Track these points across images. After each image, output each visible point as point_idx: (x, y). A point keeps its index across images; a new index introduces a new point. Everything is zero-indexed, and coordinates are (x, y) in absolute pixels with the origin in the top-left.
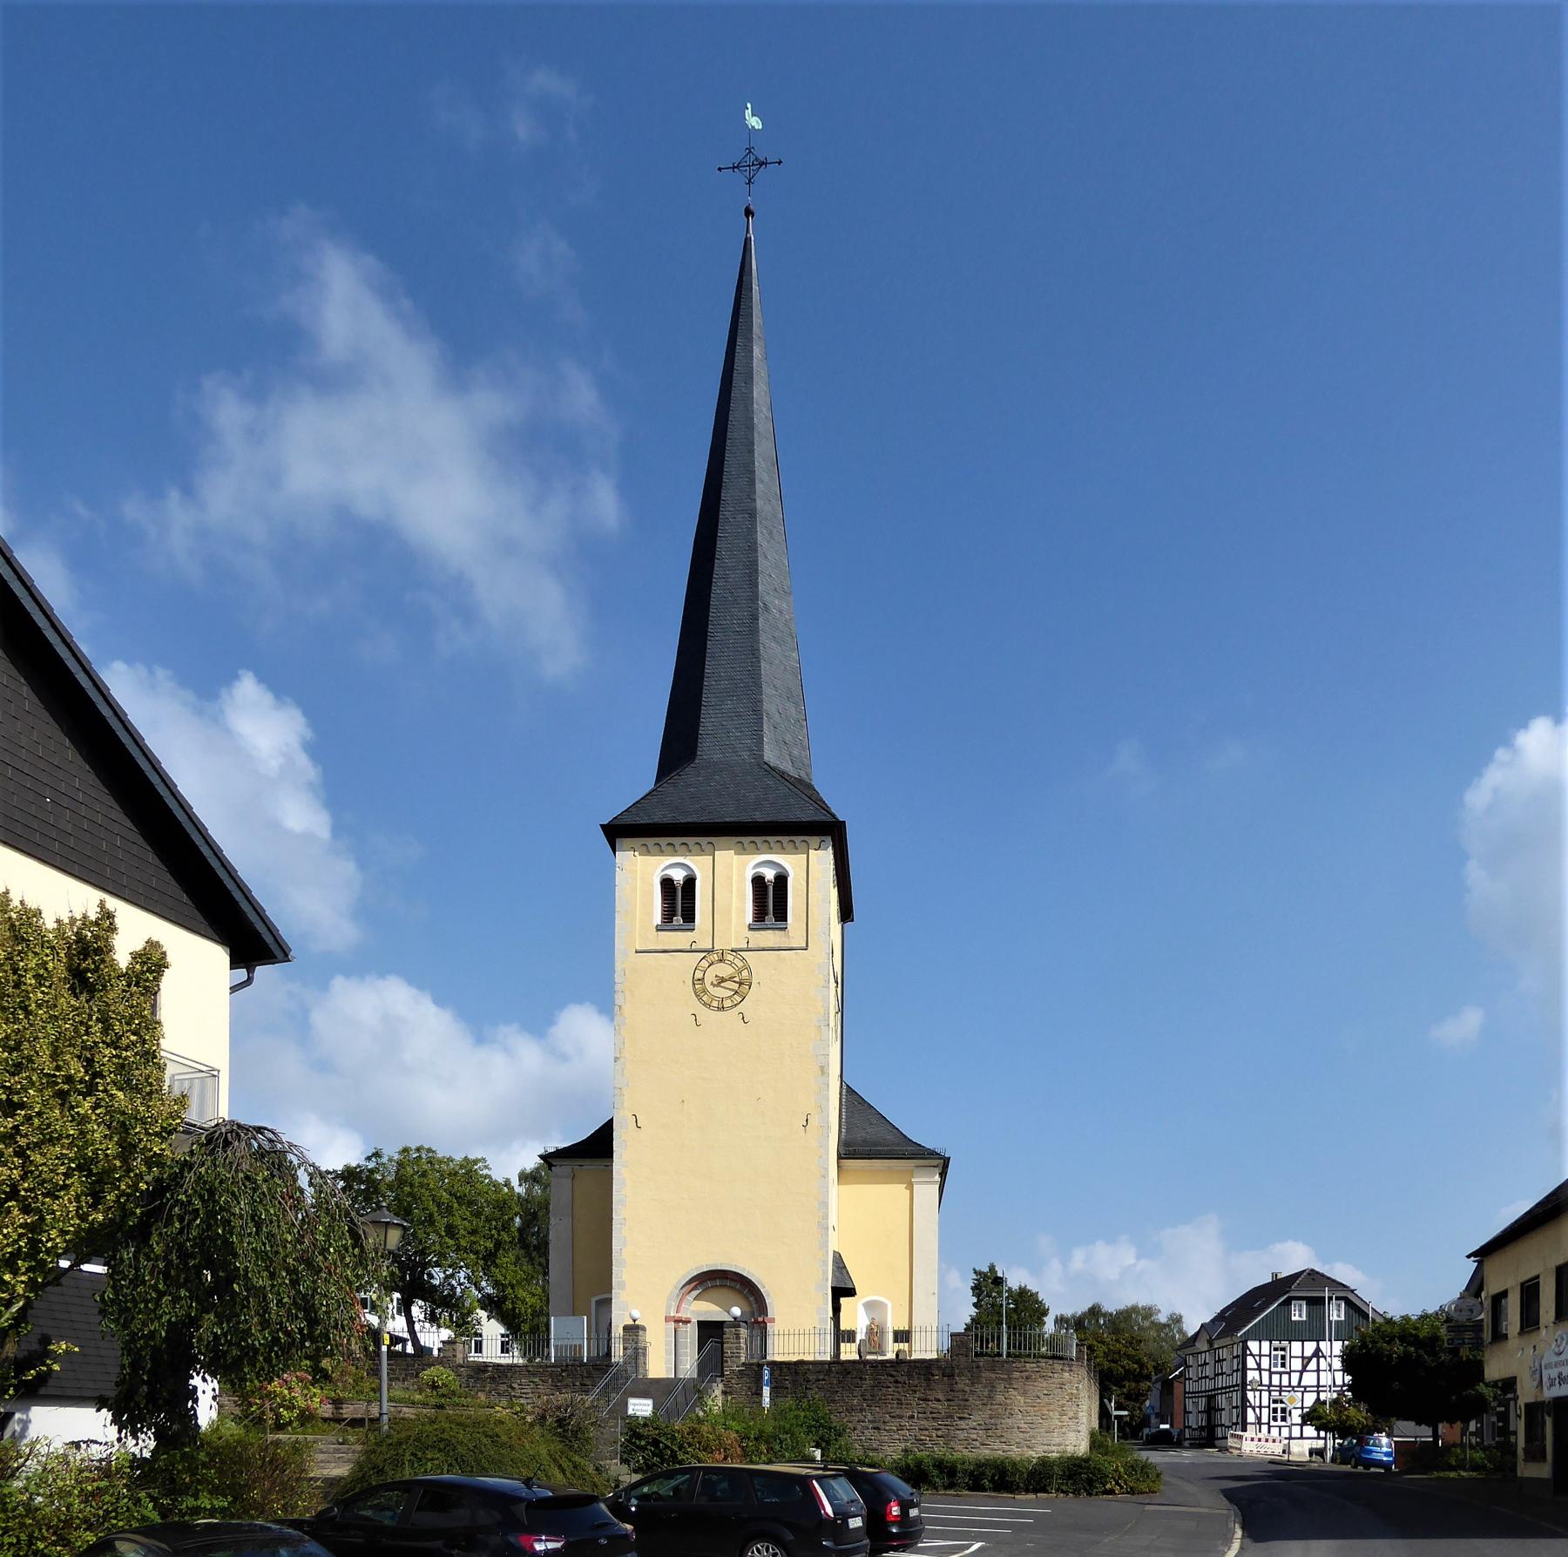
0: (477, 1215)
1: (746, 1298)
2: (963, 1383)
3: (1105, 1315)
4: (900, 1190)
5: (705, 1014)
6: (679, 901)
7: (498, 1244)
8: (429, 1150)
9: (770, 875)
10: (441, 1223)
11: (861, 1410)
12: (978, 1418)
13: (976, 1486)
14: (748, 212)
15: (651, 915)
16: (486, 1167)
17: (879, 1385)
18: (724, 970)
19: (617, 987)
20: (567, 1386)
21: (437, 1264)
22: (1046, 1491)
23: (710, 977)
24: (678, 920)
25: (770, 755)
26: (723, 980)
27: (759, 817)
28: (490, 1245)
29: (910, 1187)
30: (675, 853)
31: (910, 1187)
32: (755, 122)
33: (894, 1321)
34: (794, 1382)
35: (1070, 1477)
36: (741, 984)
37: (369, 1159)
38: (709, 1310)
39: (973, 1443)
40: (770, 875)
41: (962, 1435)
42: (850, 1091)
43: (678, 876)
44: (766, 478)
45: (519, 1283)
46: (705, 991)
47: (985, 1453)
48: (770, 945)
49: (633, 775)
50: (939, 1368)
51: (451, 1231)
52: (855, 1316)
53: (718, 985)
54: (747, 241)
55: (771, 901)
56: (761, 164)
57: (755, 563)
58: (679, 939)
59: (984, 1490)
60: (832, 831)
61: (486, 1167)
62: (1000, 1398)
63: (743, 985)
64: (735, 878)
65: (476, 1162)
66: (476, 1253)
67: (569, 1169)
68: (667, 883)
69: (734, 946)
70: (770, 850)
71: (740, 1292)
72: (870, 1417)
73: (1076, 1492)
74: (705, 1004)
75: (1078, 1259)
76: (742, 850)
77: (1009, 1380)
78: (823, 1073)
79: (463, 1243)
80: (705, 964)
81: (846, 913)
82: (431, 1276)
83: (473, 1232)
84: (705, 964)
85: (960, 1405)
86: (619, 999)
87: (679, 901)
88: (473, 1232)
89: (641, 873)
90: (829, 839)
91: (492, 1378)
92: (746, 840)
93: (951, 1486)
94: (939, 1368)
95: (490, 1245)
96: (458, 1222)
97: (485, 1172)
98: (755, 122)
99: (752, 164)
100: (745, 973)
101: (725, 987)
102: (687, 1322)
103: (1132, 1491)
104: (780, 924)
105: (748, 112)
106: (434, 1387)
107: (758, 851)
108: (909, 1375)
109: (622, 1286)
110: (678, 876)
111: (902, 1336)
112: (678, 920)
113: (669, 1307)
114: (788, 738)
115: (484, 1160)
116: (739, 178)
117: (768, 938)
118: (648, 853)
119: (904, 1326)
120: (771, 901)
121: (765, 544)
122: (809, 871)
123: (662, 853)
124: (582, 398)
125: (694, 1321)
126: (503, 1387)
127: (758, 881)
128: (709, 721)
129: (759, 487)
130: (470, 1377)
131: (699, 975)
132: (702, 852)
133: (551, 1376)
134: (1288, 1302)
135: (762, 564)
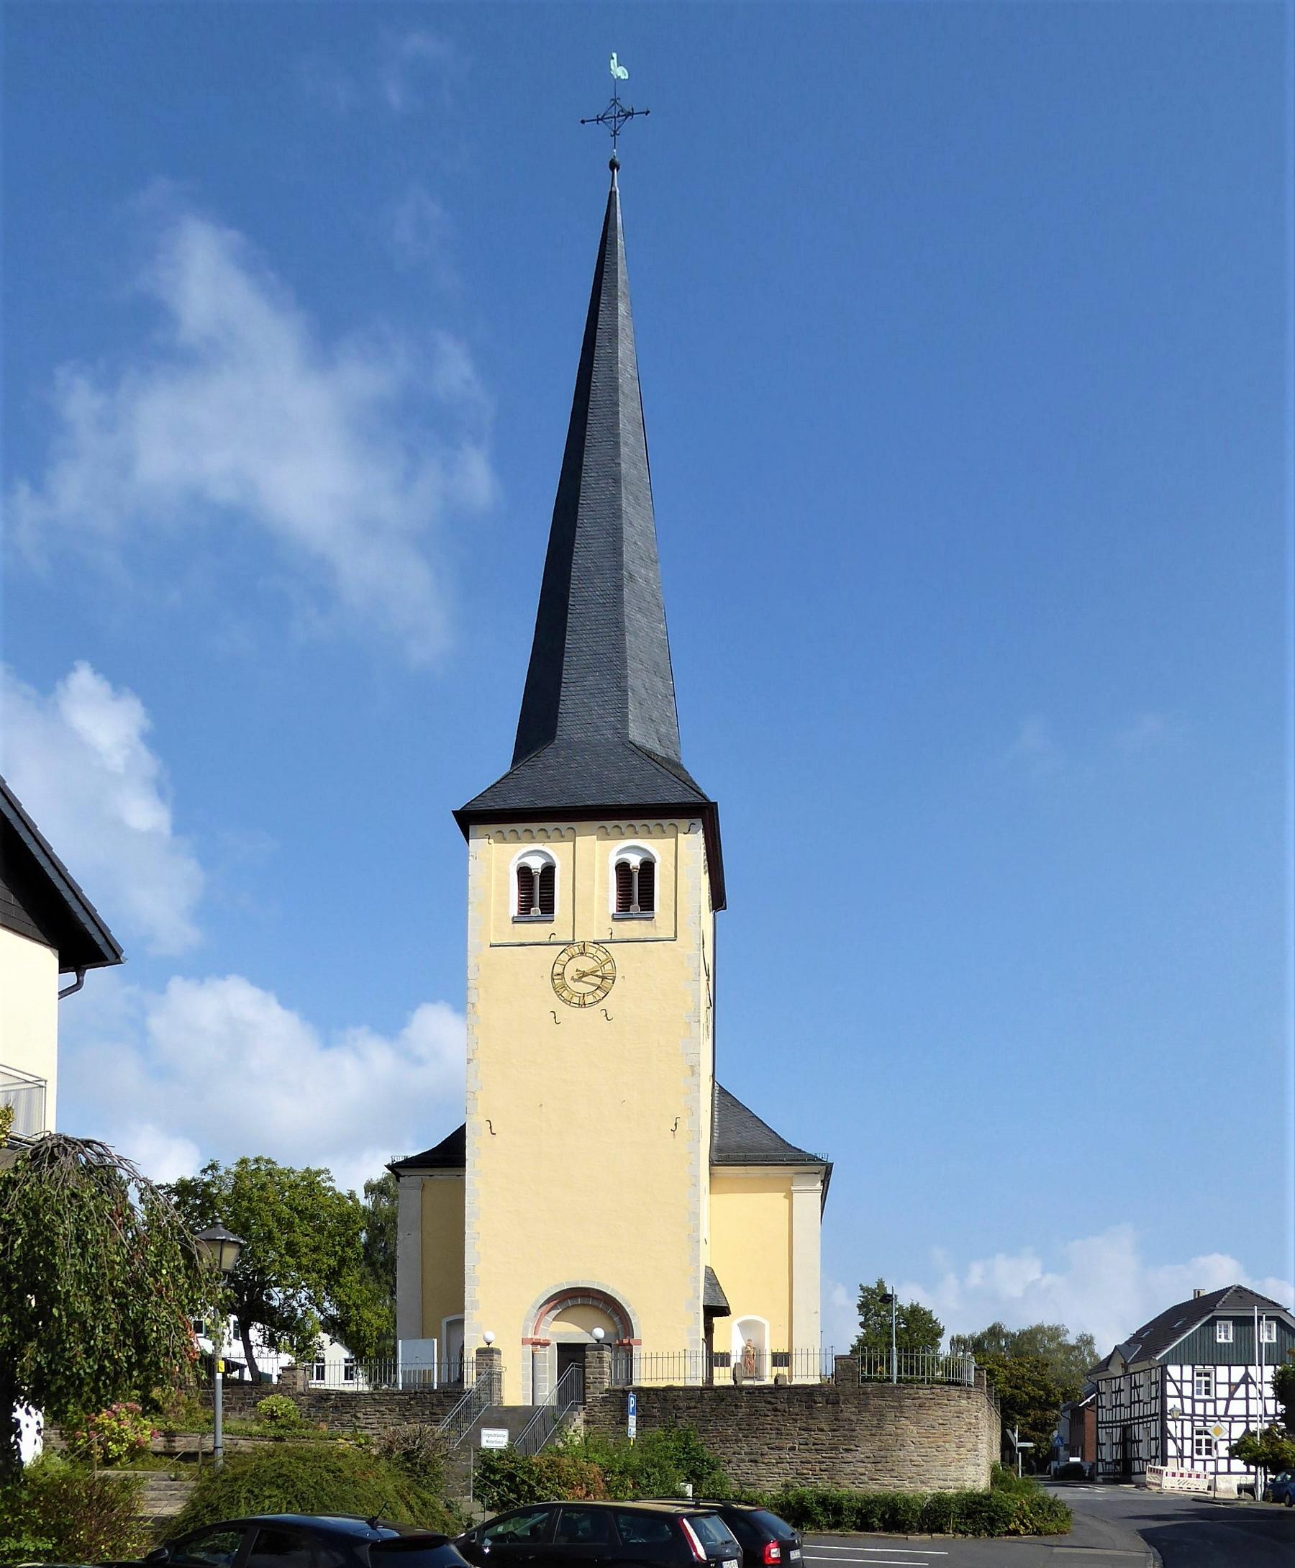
0: (320, 1230)
1: (611, 1318)
2: (848, 1411)
3: (1006, 1336)
4: (776, 1201)
5: (564, 1011)
6: (537, 891)
7: (343, 1261)
9: (635, 861)
10: (281, 1239)
11: (737, 1441)
12: (867, 1449)
13: (865, 1526)
14: (613, 165)
15: (507, 905)
16: (330, 1179)
17: (755, 1413)
18: (586, 964)
19: (470, 984)
22: (942, 1531)
23: (570, 972)
24: (536, 911)
25: (635, 733)
26: (584, 974)
27: (624, 800)
29: (789, 1195)
30: (533, 839)
31: (789, 1195)
32: (620, 72)
33: (772, 1343)
35: (969, 1516)
36: (603, 978)
37: (204, 1171)
39: (860, 1479)
40: (635, 861)
41: (848, 1469)
42: (723, 1092)
43: (536, 864)
44: (631, 440)
46: (565, 987)
47: (874, 1489)
49: (488, 759)
50: (822, 1394)
51: (291, 1249)
52: (729, 1337)
53: (579, 979)
54: (612, 195)
55: (636, 889)
57: (619, 530)
58: (537, 931)
59: (874, 1530)
60: (702, 812)
61: (330, 1179)
62: (890, 1428)
63: (606, 980)
64: (597, 864)
65: (318, 1173)
66: (319, 1271)
68: (524, 873)
69: (597, 938)
70: (636, 835)
72: (746, 1449)
73: (976, 1533)
74: (565, 1001)
75: (976, 1275)
76: (606, 836)
77: (900, 1408)
78: (693, 1074)
79: (304, 1261)
80: (564, 957)
81: (718, 901)
82: (270, 1297)
84: (564, 957)
85: (845, 1436)
86: (472, 997)
87: (537, 891)
88: (315, 1249)
89: (497, 860)
90: (699, 822)
91: (336, 1407)
93: (837, 1525)
94: (822, 1394)
97: (328, 1184)
98: (620, 72)
99: (618, 115)
100: (608, 967)
101: (587, 982)
102: (546, 1344)
103: (1038, 1532)
104: (647, 914)
105: (614, 63)
106: (273, 1417)
107: (622, 835)
108: (789, 1402)
110: (536, 864)
111: (781, 1359)
113: (526, 1328)
114: (655, 715)
115: (328, 1171)
116: (604, 129)
117: (634, 928)
118: (504, 840)
119: (783, 1348)
120: (636, 889)
121: (630, 510)
122: (678, 855)
123: (518, 839)
124: (456, 370)
125: (554, 1343)
126: (347, 1417)
127: (623, 868)
129: (624, 450)
130: (311, 1406)
131: (558, 969)
132: (562, 838)
133: (398, 1404)
135: (628, 532)
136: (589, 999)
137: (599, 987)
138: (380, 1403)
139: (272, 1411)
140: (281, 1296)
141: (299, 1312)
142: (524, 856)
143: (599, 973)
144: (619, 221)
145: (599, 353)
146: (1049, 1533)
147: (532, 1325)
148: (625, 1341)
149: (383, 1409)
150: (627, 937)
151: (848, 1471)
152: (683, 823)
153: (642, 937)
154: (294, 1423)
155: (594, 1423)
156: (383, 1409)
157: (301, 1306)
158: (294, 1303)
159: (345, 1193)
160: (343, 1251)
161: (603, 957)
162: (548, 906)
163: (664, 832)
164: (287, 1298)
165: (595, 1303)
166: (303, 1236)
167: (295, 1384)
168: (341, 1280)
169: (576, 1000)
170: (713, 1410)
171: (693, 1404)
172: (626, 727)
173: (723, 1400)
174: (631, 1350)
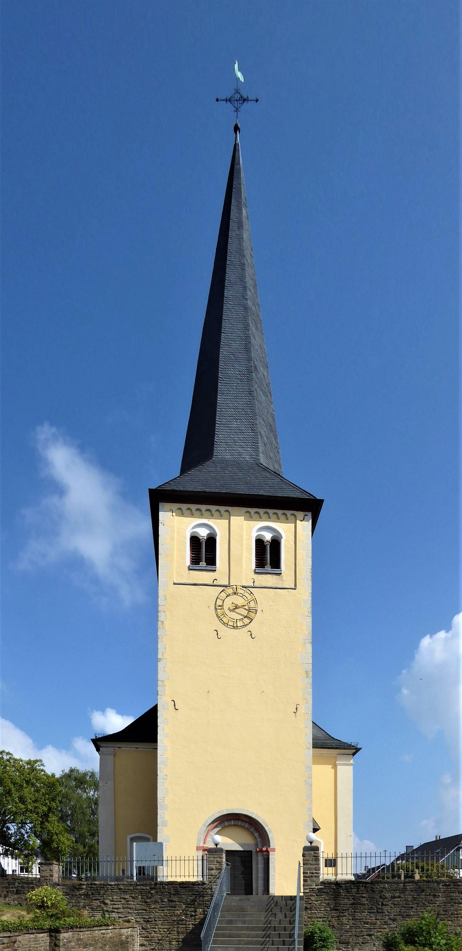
0: (37, 791)
1: (252, 834)
4: (328, 769)
6: (203, 552)
7: (50, 809)
8: (8, 753)
10: (16, 795)
14: (236, 129)
15: (185, 558)
16: (43, 765)
17: (451, 901)
19: (160, 608)
20: (156, 902)
21: (13, 821)
23: (228, 603)
24: (203, 564)
25: (263, 460)
26: (237, 607)
28: (45, 809)
29: (335, 767)
30: (202, 516)
31: (335, 767)
34: (371, 899)
36: (249, 610)
38: (228, 842)
43: (203, 533)
45: (61, 833)
46: (224, 614)
48: (270, 585)
49: (166, 469)
51: (22, 800)
54: (236, 145)
55: (268, 555)
56: (244, 100)
58: (205, 577)
61: (43, 765)
63: (250, 614)
65: (36, 761)
66: (37, 813)
67: (112, 750)
69: (244, 585)
70: (269, 519)
71: (247, 829)
74: (224, 624)
76: (250, 518)
79: (30, 807)
82: (8, 828)
83: (35, 801)
84: (223, 595)
87: (203, 552)
89: (179, 527)
90: (310, 514)
91: (87, 895)
92: (253, 510)
95: (45, 809)
96: (26, 795)
97: (42, 767)
99: (238, 99)
104: (276, 571)
106: (42, 906)
107: (260, 519)
109: (165, 824)
110: (203, 533)
111: (331, 863)
112: (203, 564)
113: (199, 840)
115: (41, 761)
118: (183, 515)
119: (331, 856)
120: (268, 555)
122: (295, 534)
123: (192, 515)
126: (96, 903)
127: (260, 542)
128: (221, 435)
131: (219, 602)
132: (221, 517)
133: (141, 893)
134: (458, 850)
136: (239, 624)
137: (245, 617)
138: (125, 892)
139: (43, 902)
140: (15, 827)
141: (26, 836)
142: (193, 528)
143: (246, 607)
144: (241, 162)
145: (232, 234)
146: (204, 920)
147: (202, 838)
148: (264, 849)
149: (127, 897)
150: (264, 585)
151: (98, 901)
152: (300, 514)
153: (274, 586)
154: (63, 912)
155: (311, 909)
156: (127, 897)
157: (27, 833)
158: (23, 831)
159: (50, 774)
160: (50, 803)
161: (249, 597)
162: (211, 561)
163: (287, 519)
164: (19, 828)
165: (243, 824)
166: (28, 792)
167: (52, 876)
168: (49, 819)
169: (231, 623)
170: (415, 899)
171: (397, 895)
172: (258, 455)
173: (423, 891)
174: (268, 856)
